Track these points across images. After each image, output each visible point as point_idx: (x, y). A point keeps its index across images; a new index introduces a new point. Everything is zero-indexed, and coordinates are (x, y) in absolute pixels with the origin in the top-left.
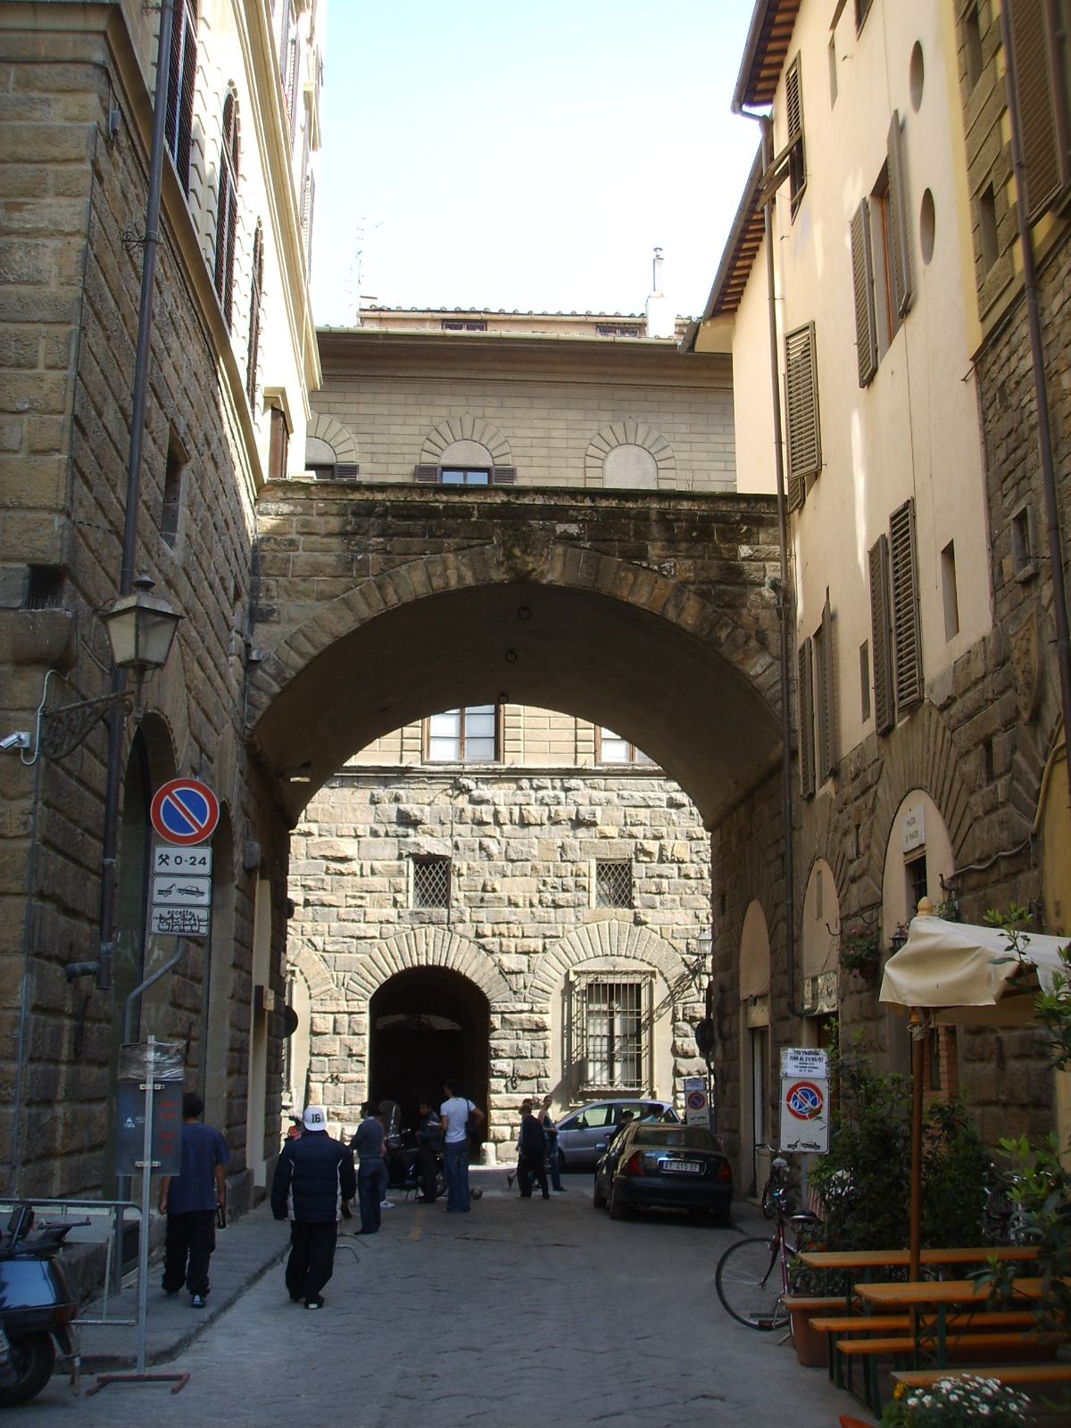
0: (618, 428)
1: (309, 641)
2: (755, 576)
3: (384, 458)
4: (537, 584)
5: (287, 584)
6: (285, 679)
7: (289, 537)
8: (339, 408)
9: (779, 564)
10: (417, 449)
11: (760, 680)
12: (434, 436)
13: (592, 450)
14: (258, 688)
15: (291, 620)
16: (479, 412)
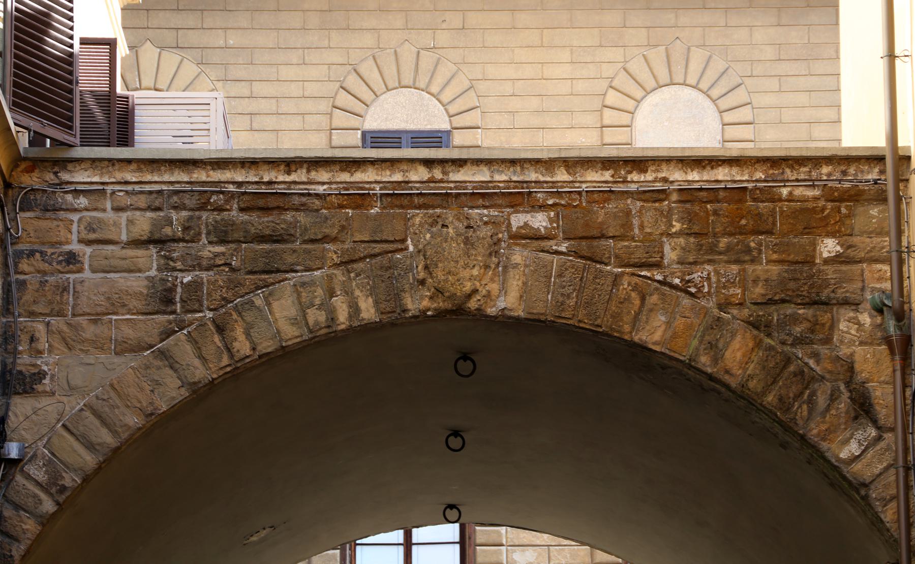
0: (657, 56)
1: (104, 422)
2: (850, 289)
3: (270, 122)
4: (480, 316)
5: (65, 328)
6: (63, 489)
7: (67, 248)
8: (194, 38)
9: (886, 268)
10: (324, 106)
11: (857, 467)
12: (352, 82)
13: (612, 98)
14: (17, 507)
15: (72, 389)
16: (426, 39)
